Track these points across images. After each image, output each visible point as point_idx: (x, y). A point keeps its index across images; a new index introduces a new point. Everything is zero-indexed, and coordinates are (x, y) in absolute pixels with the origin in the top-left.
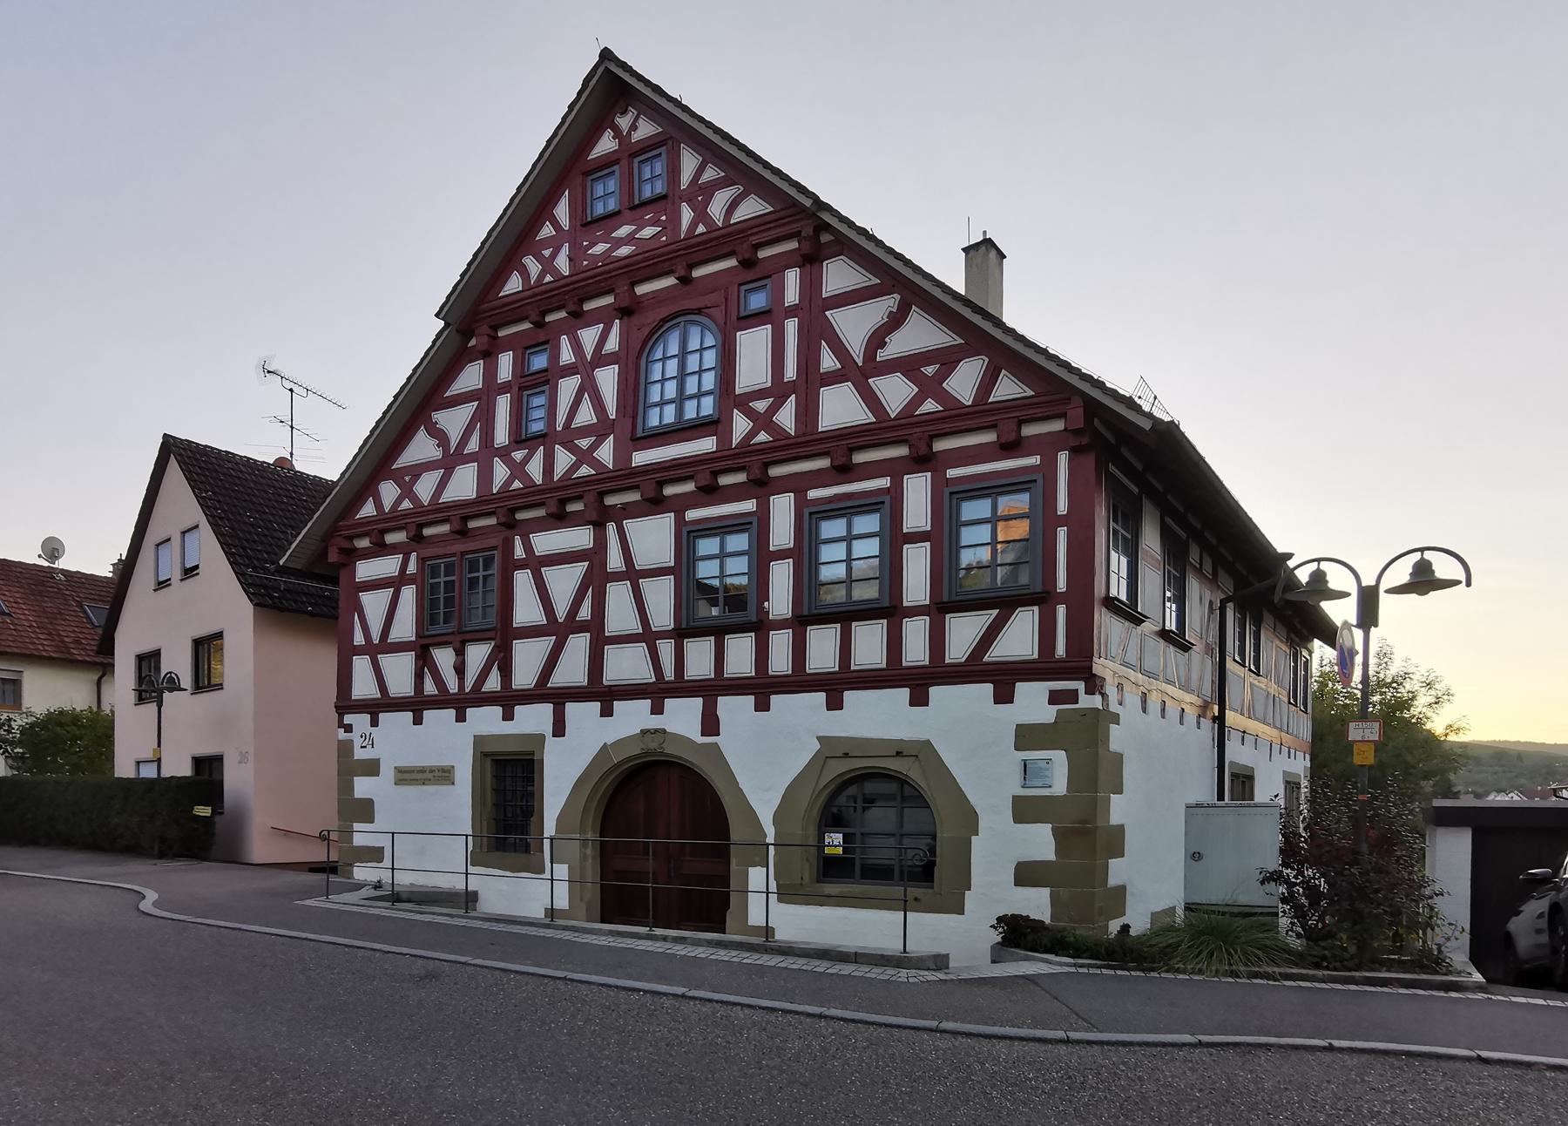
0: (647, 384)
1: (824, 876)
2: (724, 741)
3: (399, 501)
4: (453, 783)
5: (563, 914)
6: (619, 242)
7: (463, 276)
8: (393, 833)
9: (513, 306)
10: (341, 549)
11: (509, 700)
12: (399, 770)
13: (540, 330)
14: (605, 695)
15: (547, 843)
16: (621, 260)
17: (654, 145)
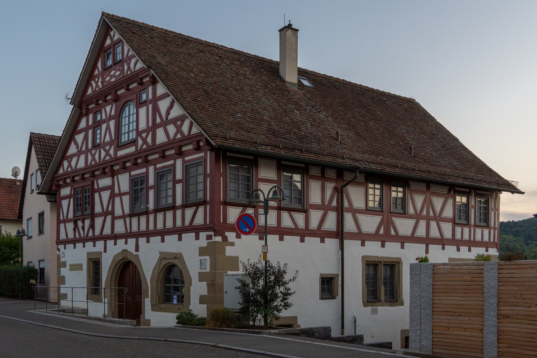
0: (121, 127)
1: (166, 301)
2: (141, 254)
3: (176, 135)
4: (82, 270)
5: (108, 316)
6: (112, 77)
7: (75, 89)
8: (72, 288)
9: (89, 99)
10: (56, 185)
11: (94, 239)
12: (71, 265)
13: (98, 106)
14: (115, 237)
15: (103, 289)
16: (113, 83)
17: (118, 42)
